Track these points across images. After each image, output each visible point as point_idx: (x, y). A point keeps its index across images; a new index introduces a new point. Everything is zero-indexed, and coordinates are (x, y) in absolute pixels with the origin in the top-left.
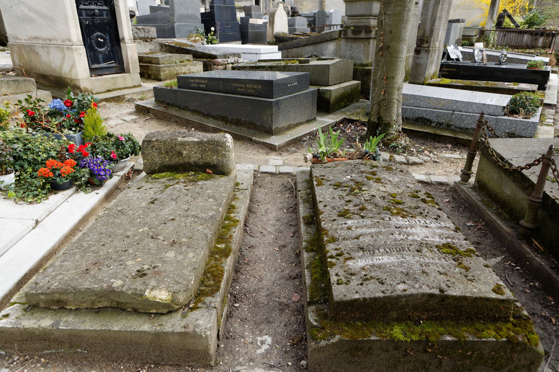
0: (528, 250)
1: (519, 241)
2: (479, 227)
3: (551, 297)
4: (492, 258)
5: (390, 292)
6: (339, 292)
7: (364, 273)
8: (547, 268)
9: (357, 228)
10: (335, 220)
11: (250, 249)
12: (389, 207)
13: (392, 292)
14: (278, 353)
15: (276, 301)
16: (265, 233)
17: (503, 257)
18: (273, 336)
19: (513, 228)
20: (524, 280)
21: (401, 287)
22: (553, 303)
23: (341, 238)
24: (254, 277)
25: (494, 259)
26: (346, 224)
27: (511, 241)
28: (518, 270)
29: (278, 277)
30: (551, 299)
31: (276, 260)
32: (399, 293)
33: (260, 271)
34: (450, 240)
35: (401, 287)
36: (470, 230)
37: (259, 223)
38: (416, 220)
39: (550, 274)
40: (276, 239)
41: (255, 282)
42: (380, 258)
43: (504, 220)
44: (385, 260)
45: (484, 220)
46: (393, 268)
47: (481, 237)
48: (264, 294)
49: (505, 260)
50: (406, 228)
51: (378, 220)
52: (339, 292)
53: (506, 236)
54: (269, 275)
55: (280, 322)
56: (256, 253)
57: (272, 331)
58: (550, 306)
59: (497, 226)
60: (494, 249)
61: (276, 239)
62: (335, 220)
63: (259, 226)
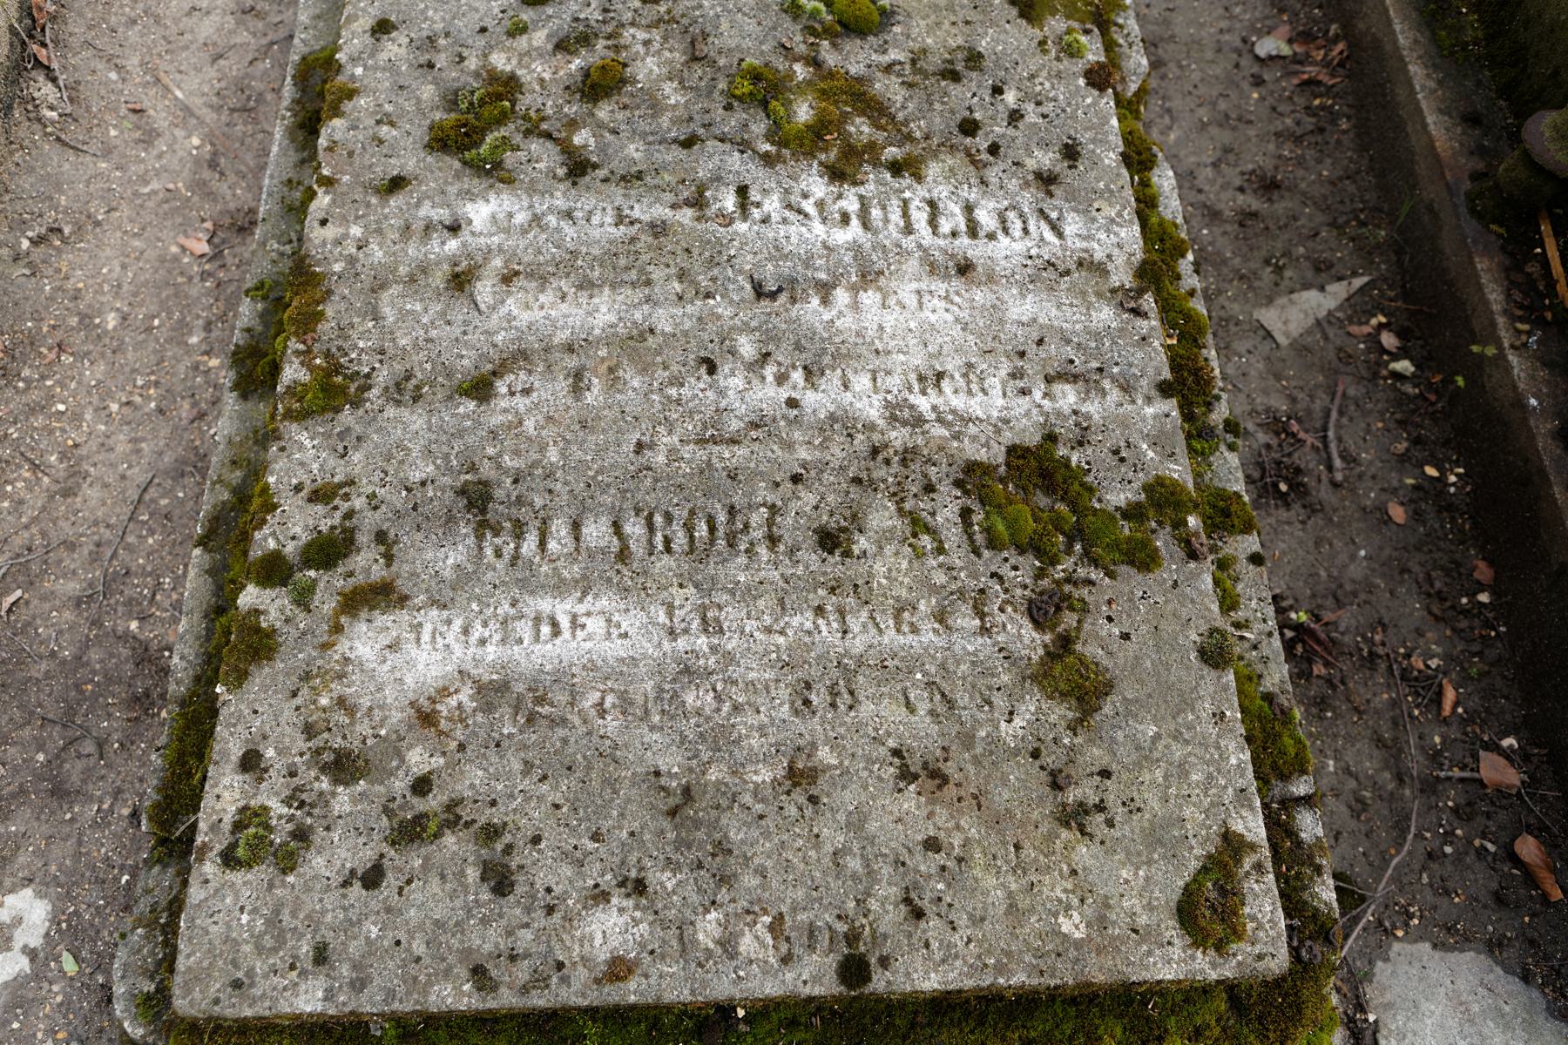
0: (1495, 296)
1: (1470, 227)
2: (1311, 71)
3: (1491, 563)
4: (1306, 286)
5: (522, 972)
6: (182, 1004)
7: (419, 759)
8: (1543, 430)
9: (507, 279)
10: (397, 184)
11: (38, 253)
12: (781, 64)
13: (540, 980)
14: (66, 1007)
15: (126, 637)
16: (160, 117)
17: (1358, 282)
18: (60, 888)
19: (1472, 119)
20: (1402, 447)
21: (610, 929)
22: (1484, 598)
23: (382, 377)
24: (35, 467)
25: (1312, 296)
26: (454, 229)
27: (1430, 208)
28: (1397, 376)
29: (168, 459)
30: (1483, 572)
31: (183, 328)
32: (575, 992)
33: (77, 418)
34: (1068, 397)
35: (610, 929)
36: (1258, 82)
37: (133, 34)
38: (917, 196)
39: (1542, 471)
40: (213, 164)
41: (35, 501)
42: (562, 609)
43: (1448, 56)
44: (596, 635)
45: (1347, 33)
46: (612, 724)
47: (1298, 140)
48: (73, 587)
49: (1357, 308)
50: (825, 291)
51: (661, 212)
52: (182, 1004)
53: (1422, 168)
54: (121, 445)
55: (117, 793)
56: (77, 281)
57: (62, 852)
58: (1465, 612)
59: (1401, 94)
60: (1333, 224)
61: (213, 164)
62: (397, 184)
63: (132, 62)
